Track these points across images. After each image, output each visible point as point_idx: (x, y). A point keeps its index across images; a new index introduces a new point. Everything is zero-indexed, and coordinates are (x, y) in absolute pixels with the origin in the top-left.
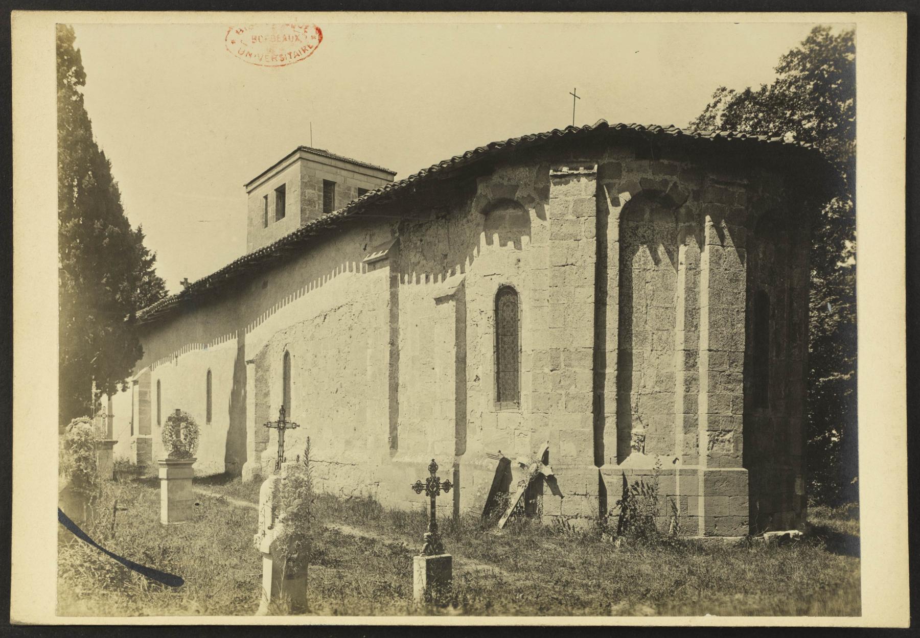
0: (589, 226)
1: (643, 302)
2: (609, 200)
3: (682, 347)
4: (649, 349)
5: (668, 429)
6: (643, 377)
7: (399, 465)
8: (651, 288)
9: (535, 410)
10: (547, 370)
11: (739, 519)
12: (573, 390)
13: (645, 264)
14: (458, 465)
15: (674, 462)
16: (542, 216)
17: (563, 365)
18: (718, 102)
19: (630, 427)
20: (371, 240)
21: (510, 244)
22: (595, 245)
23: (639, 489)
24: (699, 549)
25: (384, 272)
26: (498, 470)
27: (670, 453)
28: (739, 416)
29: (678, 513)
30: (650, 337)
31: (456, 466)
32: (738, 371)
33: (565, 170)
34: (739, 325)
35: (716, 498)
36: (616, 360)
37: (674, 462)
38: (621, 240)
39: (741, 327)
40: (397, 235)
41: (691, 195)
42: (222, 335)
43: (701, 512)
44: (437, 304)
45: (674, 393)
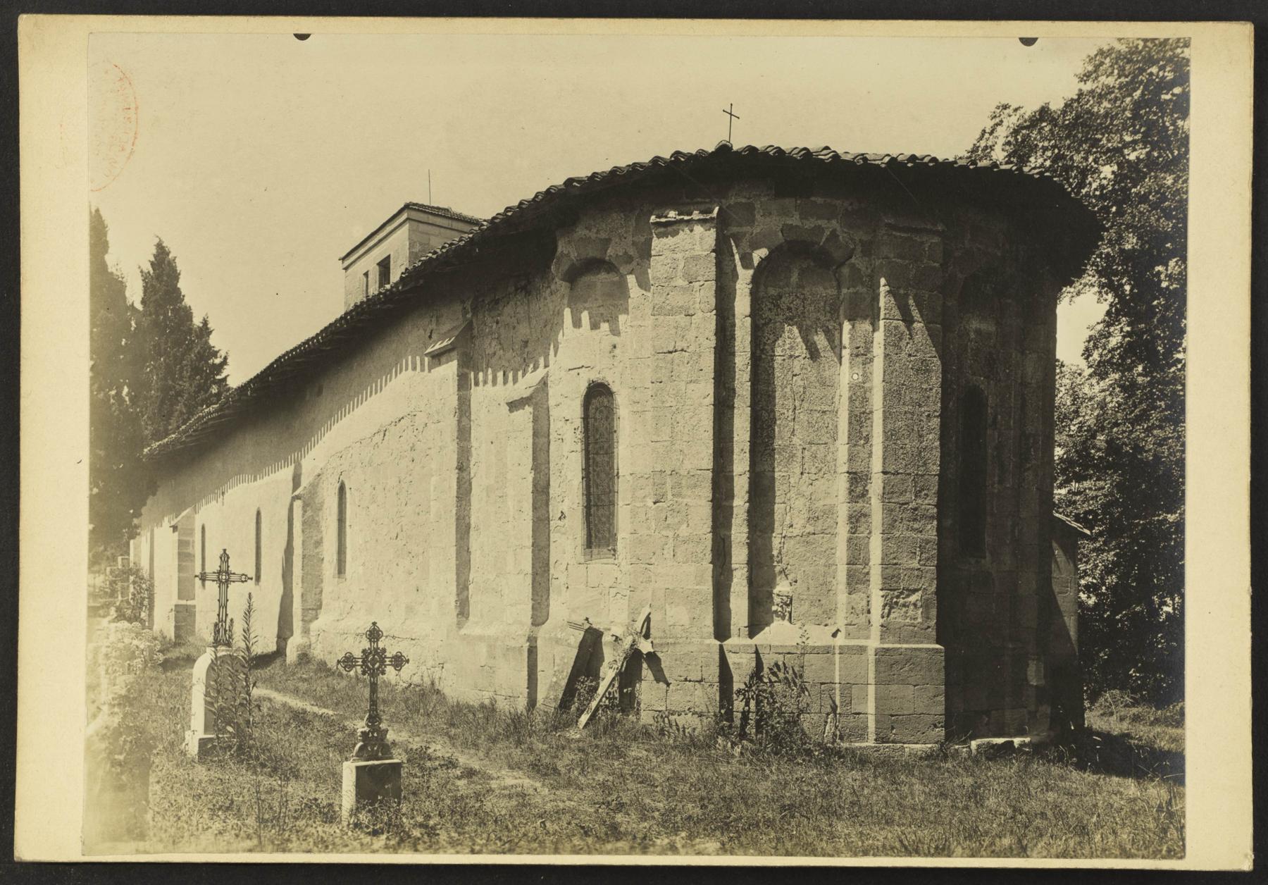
0: (706, 294)
1: (789, 403)
2: (737, 257)
3: (846, 469)
4: (798, 471)
5: (826, 588)
6: (790, 512)
7: (465, 638)
8: (801, 383)
9: (634, 560)
10: (650, 503)
11: (930, 719)
12: (684, 531)
13: (791, 348)
14: (536, 639)
15: (834, 635)
16: (644, 284)
17: (670, 497)
18: (997, 125)
19: (771, 583)
20: (438, 323)
21: (605, 326)
22: (714, 323)
23: (781, 675)
24: (861, 761)
25: (450, 368)
26: (582, 645)
27: (829, 622)
28: (931, 568)
29: (839, 711)
30: (799, 454)
31: (532, 640)
32: (929, 504)
33: (672, 214)
34: (931, 437)
35: (894, 687)
36: (746, 487)
37: (834, 635)
38: (753, 315)
39: (933, 440)
40: (469, 316)
41: (859, 249)
42: (277, 459)
43: (871, 708)
44: (511, 411)
45: (834, 535)
